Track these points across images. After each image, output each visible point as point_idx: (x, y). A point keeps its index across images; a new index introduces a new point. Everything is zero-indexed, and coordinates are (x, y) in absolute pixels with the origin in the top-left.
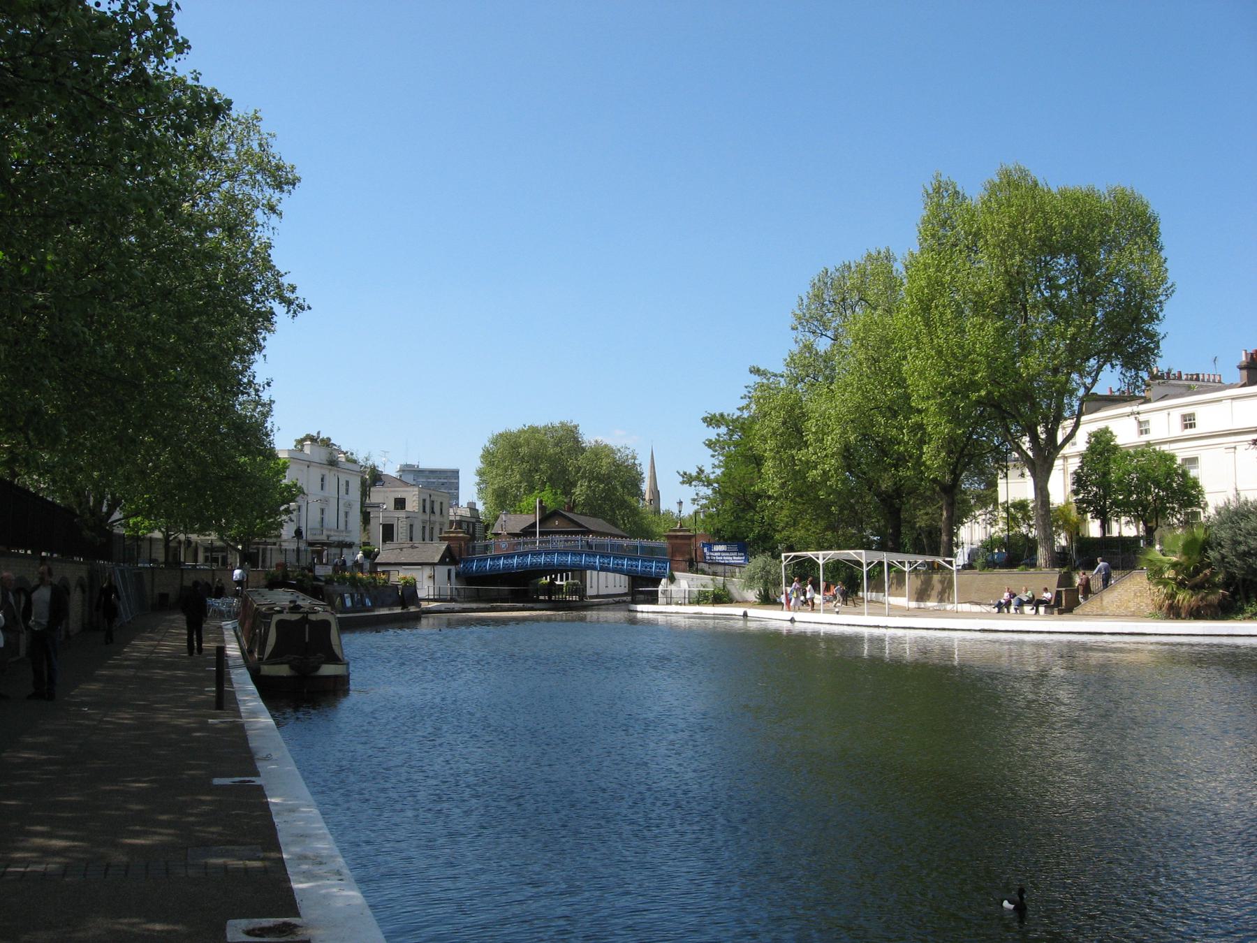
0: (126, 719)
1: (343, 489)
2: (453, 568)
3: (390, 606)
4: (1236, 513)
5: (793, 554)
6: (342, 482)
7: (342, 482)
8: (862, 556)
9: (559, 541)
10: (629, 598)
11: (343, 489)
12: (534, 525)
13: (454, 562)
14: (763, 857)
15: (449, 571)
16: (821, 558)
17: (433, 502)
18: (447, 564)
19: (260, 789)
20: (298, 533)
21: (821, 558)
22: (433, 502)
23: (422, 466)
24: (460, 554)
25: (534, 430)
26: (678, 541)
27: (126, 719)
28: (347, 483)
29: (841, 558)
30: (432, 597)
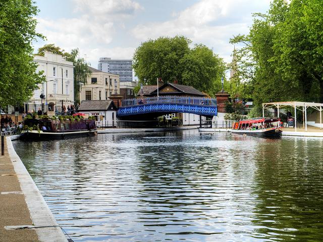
0: (70, 230)
1: (64, 74)
2: (115, 112)
3: (82, 129)
4: (192, 66)
5: (267, 104)
6: (64, 71)
7: (64, 71)
8: (295, 104)
9: (169, 99)
10: (199, 126)
11: (64, 74)
12: (156, 91)
13: (115, 109)
14: (211, 223)
15: (113, 113)
16: (278, 105)
17: (111, 79)
18: (112, 110)
19: (23, 196)
20: (42, 96)
21: (278, 105)
22: (111, 79)
23: (112, 59)
24: (118, 105)
25: (164, 41)
26: (220, 98)
27: (70, 230)
28: (67, 71)
29: (311, 106)
30: (105, 126)
